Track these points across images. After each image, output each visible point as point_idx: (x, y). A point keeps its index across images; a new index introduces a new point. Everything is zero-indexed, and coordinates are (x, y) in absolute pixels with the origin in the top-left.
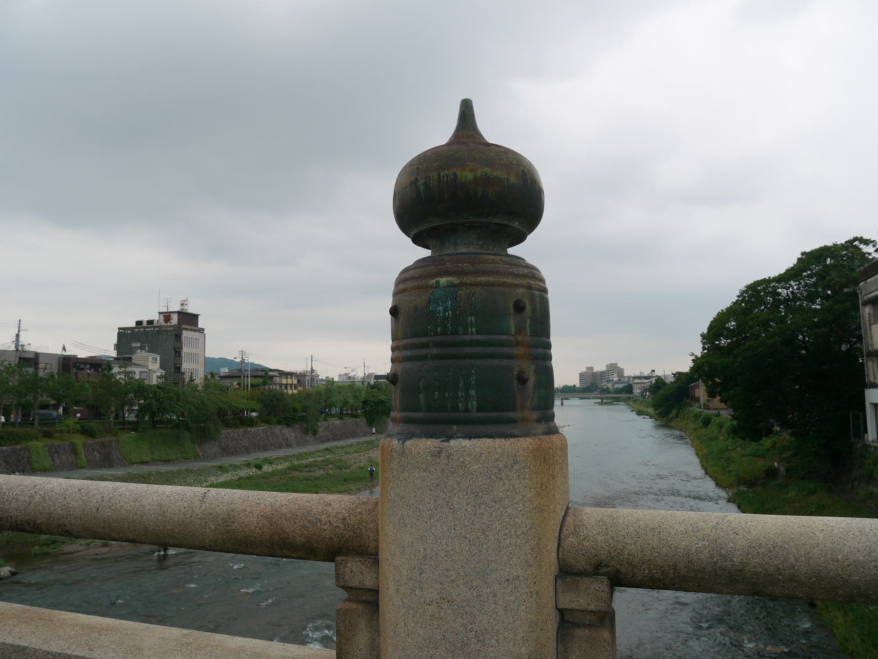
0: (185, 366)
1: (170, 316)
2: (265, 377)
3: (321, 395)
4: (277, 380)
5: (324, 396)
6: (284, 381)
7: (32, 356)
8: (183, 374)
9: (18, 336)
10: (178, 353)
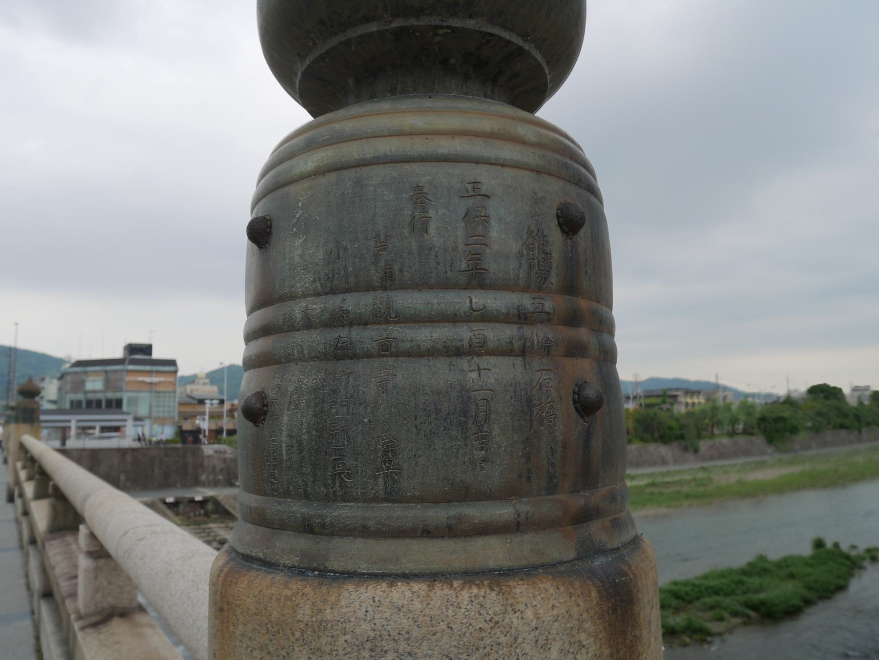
6: (689, 401)
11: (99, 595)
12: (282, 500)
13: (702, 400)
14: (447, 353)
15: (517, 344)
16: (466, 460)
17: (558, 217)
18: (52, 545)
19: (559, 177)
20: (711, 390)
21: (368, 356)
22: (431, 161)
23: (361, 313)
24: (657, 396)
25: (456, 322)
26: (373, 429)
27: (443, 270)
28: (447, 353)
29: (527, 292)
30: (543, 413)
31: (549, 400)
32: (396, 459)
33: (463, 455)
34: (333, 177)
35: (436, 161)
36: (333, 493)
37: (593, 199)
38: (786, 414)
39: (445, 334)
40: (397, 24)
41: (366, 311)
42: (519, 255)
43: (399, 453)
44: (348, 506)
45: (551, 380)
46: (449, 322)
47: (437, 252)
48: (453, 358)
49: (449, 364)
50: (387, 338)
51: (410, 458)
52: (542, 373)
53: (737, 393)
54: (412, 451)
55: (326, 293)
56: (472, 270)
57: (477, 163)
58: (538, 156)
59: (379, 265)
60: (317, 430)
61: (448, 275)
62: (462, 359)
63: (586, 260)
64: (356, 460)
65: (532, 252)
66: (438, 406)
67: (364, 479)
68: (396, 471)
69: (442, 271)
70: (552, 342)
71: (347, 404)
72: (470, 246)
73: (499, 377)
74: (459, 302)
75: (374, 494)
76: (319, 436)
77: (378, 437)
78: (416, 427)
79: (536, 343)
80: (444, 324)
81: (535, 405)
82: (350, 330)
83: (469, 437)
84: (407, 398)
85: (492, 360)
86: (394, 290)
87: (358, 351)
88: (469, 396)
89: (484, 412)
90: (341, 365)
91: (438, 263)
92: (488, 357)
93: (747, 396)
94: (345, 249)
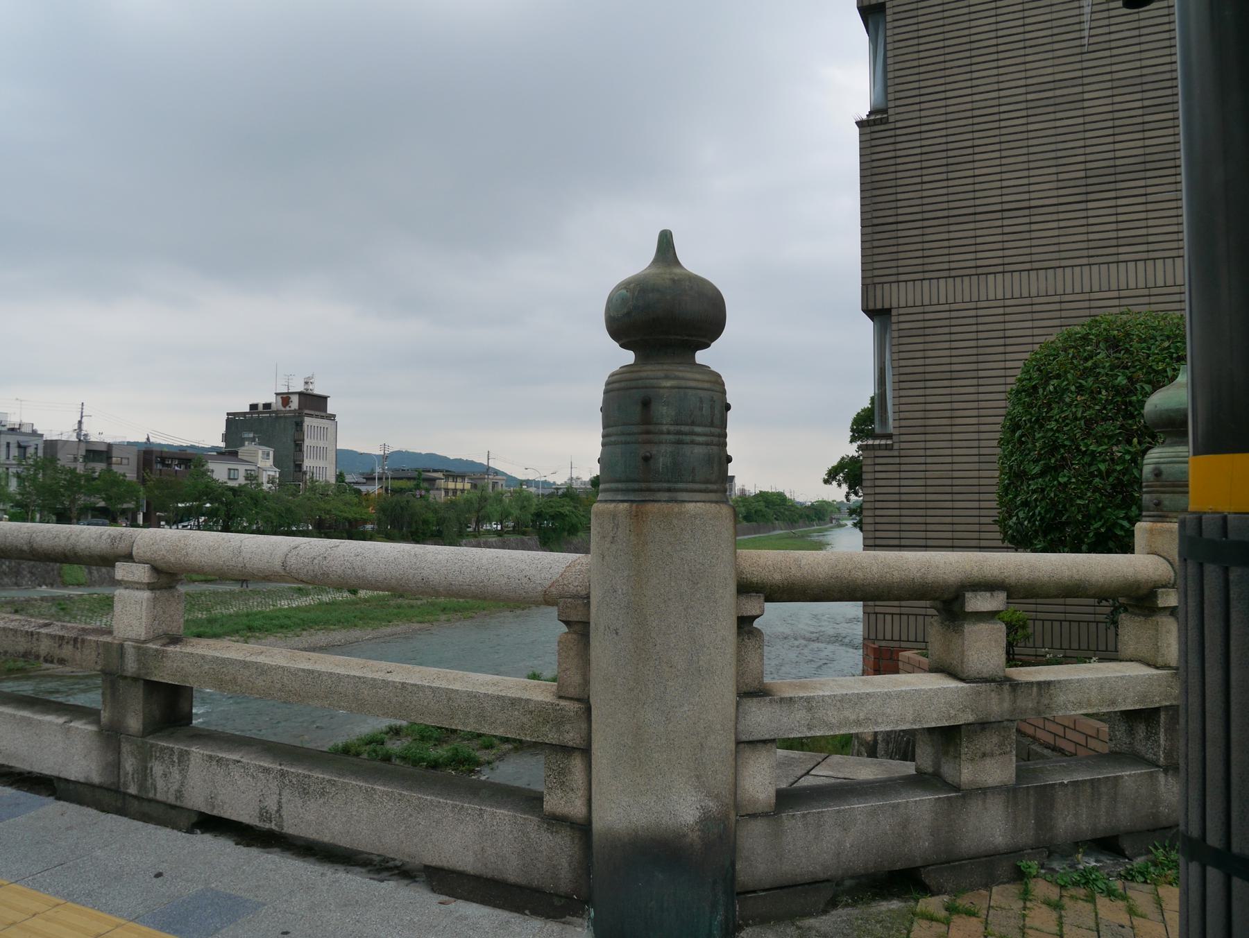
0: (308, 463)
1: (290, 398)
2: (419, 479)
3: (471, 503)
4: (442, 483)
5: (476, 505)
6: (451, 485)
7: (104, 448)
8: (305, 473)
9: (80, 422)
10: (298, 446)
13: (468, 486)
20: (478, 474)
21: (687, 443)
24: (409, 479)
34: (677, 390)
38: (566, 510)
40: (686, 338)
53: (510, 479)
90: (680, 446)
93: (522, 483)
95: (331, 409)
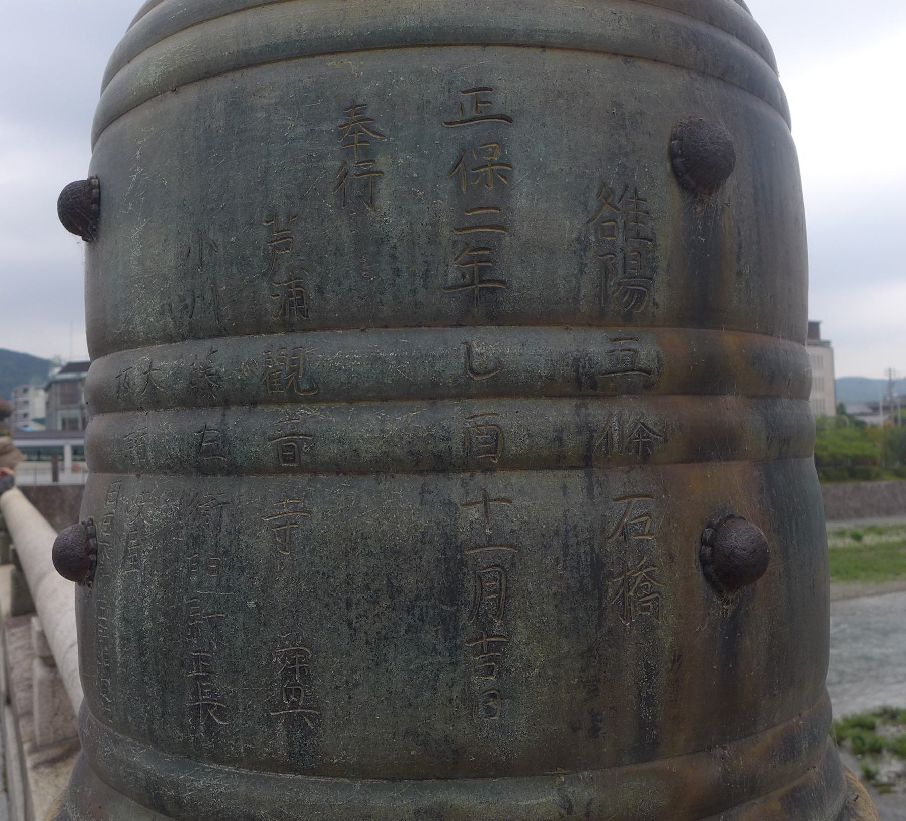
11: (60, 718)
12: (120, 736)
14: (417, 465)
15: (573, 443)
16: (455, 694)
17: (673, 155)
18: (13, 635)
19: (677, 66)
21: (258, 469)
22: (383, 48)
23: (243, 380)
25: (436, 399)
26: (265, 625)
27: (409, 287)
28: (417, 465)
29: (597, 326)
30: (629, 590)
31: (642, 563)
32: (309, 688)
33: (447, 684)
34: (191, 94)
35: (394, 48)
36: (194, 742)
37: (762, 108)
39: (412, 425)
41: (253, 377)
42: (578, 246)
43: (315, 677)
44: (221, 772)
45: (651, 517)
46: (423, 399)
47: (395, 247)
48: (431, 476)
49: (419, 490)
50: (293, 435)
51: (337, 687)
52: (629, 503)
54: (340, 673)
55: (183, 336)
56: (472, 284)
57: (485, 45)
58: (627, 19)
59: (276, 279)
60: (166, 615)
61: (419, 297)
62: (449, 479)
63: (740, 246)
64: (233, 683)
65: (609, 238)
66: (394, 581)
67: (249, 722)
68: (309, 711)
69: (406, 288)
70: (654, 433)
71: (217, 569)
72: (467, 232)
73: (530, 517)
74: (442, 356)
75: (268, 753)
76: (169, 627)
77: (275, 641)
78: (350, 624)
79: (616, 438)
80: (410, 403)
81: (610, 575)
82: (224, 415)
83: (460, 648)
84: (332, 563)
85: (516, 478)
86: (309, 330)
87: (238, 459)
88: (462, 559)
89: (494, 593)
91: (397, 272)
92: (507, 473)
94: (211, 245)
95: (824, 335)
